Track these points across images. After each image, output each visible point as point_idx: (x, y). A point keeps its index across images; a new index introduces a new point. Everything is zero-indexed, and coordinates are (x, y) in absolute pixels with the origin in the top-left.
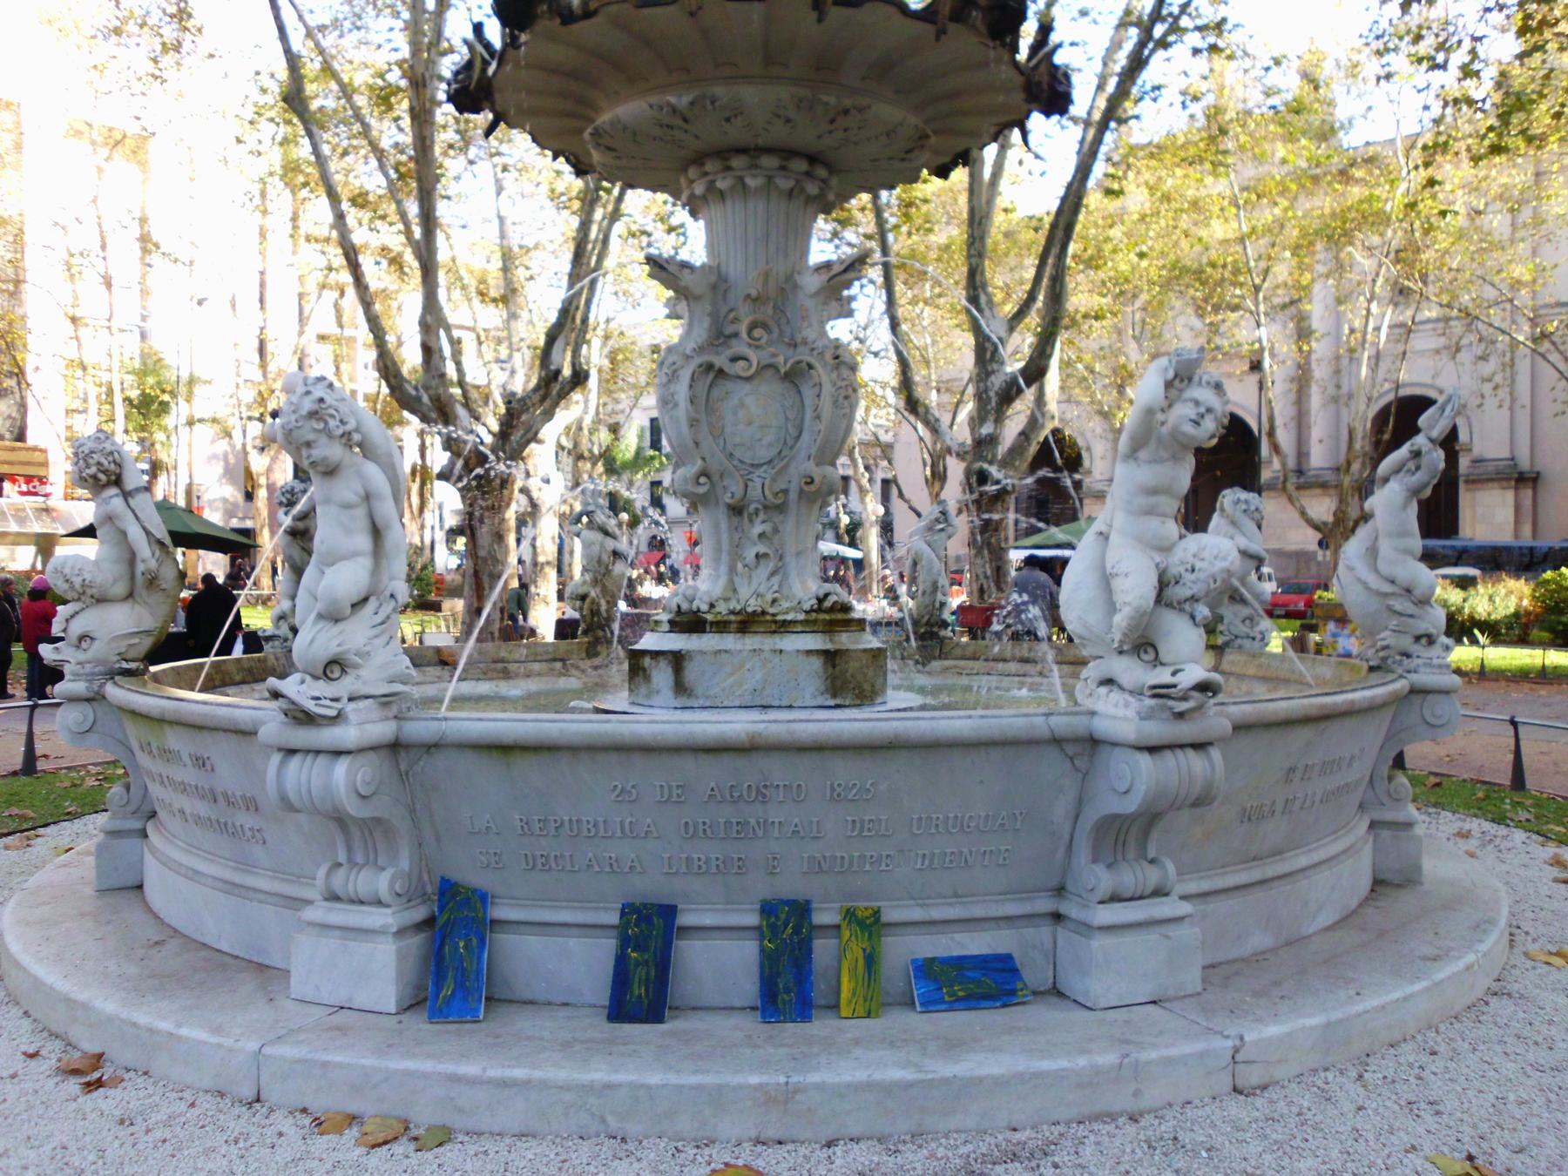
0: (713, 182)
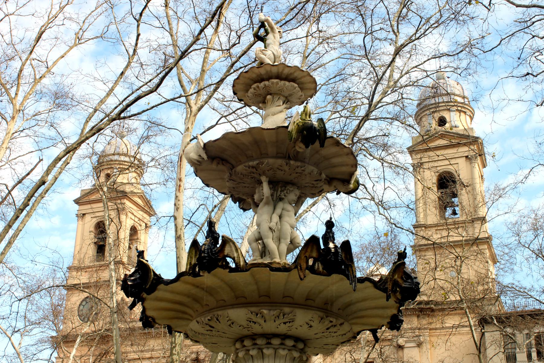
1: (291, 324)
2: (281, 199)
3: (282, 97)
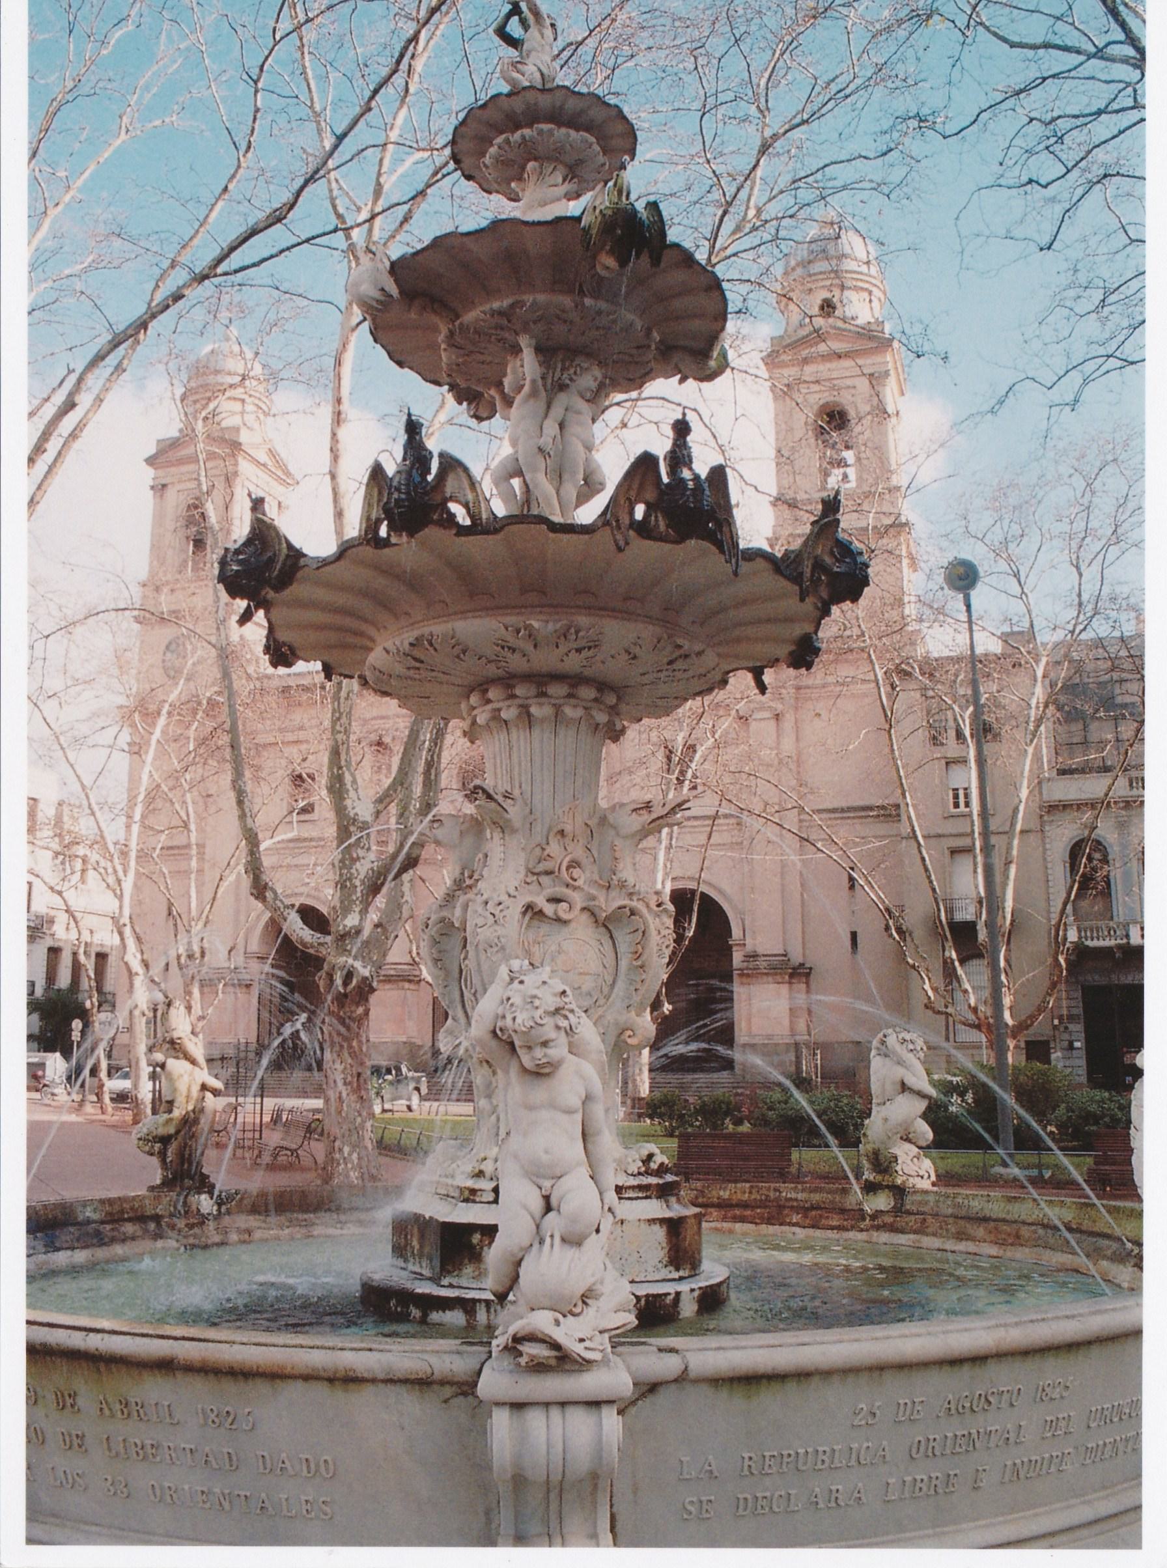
0: (499, 710)
1: (591, 653)
2: (562, 387)
3: (560, 167)
